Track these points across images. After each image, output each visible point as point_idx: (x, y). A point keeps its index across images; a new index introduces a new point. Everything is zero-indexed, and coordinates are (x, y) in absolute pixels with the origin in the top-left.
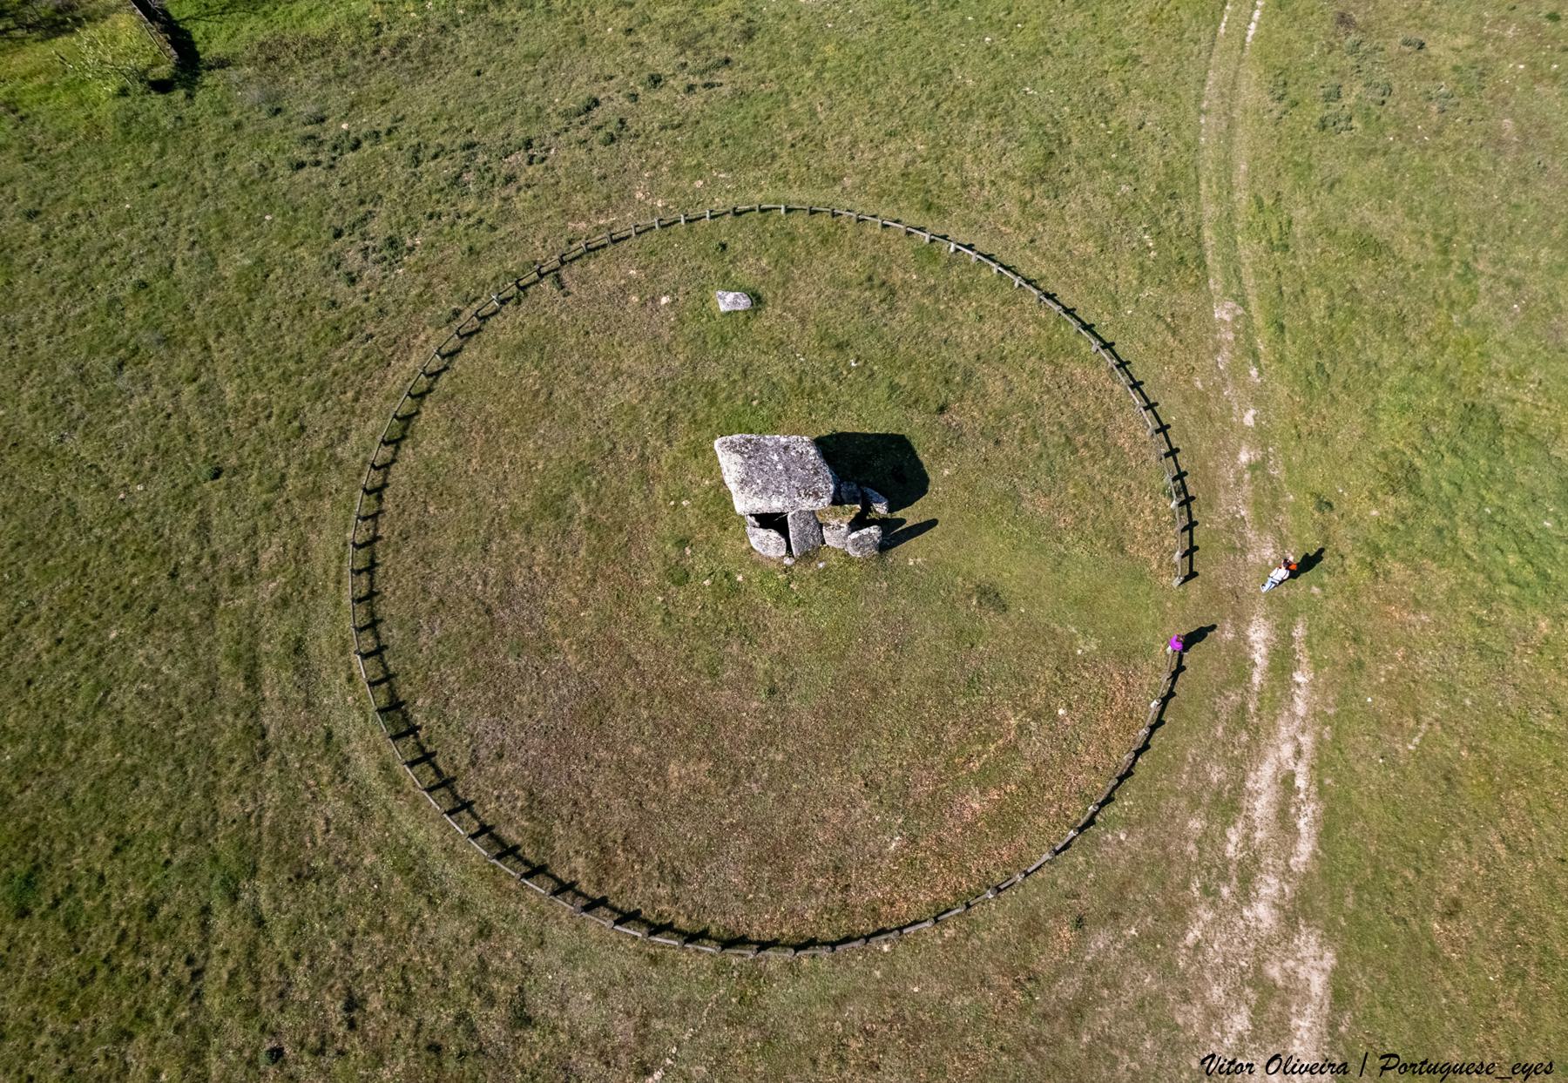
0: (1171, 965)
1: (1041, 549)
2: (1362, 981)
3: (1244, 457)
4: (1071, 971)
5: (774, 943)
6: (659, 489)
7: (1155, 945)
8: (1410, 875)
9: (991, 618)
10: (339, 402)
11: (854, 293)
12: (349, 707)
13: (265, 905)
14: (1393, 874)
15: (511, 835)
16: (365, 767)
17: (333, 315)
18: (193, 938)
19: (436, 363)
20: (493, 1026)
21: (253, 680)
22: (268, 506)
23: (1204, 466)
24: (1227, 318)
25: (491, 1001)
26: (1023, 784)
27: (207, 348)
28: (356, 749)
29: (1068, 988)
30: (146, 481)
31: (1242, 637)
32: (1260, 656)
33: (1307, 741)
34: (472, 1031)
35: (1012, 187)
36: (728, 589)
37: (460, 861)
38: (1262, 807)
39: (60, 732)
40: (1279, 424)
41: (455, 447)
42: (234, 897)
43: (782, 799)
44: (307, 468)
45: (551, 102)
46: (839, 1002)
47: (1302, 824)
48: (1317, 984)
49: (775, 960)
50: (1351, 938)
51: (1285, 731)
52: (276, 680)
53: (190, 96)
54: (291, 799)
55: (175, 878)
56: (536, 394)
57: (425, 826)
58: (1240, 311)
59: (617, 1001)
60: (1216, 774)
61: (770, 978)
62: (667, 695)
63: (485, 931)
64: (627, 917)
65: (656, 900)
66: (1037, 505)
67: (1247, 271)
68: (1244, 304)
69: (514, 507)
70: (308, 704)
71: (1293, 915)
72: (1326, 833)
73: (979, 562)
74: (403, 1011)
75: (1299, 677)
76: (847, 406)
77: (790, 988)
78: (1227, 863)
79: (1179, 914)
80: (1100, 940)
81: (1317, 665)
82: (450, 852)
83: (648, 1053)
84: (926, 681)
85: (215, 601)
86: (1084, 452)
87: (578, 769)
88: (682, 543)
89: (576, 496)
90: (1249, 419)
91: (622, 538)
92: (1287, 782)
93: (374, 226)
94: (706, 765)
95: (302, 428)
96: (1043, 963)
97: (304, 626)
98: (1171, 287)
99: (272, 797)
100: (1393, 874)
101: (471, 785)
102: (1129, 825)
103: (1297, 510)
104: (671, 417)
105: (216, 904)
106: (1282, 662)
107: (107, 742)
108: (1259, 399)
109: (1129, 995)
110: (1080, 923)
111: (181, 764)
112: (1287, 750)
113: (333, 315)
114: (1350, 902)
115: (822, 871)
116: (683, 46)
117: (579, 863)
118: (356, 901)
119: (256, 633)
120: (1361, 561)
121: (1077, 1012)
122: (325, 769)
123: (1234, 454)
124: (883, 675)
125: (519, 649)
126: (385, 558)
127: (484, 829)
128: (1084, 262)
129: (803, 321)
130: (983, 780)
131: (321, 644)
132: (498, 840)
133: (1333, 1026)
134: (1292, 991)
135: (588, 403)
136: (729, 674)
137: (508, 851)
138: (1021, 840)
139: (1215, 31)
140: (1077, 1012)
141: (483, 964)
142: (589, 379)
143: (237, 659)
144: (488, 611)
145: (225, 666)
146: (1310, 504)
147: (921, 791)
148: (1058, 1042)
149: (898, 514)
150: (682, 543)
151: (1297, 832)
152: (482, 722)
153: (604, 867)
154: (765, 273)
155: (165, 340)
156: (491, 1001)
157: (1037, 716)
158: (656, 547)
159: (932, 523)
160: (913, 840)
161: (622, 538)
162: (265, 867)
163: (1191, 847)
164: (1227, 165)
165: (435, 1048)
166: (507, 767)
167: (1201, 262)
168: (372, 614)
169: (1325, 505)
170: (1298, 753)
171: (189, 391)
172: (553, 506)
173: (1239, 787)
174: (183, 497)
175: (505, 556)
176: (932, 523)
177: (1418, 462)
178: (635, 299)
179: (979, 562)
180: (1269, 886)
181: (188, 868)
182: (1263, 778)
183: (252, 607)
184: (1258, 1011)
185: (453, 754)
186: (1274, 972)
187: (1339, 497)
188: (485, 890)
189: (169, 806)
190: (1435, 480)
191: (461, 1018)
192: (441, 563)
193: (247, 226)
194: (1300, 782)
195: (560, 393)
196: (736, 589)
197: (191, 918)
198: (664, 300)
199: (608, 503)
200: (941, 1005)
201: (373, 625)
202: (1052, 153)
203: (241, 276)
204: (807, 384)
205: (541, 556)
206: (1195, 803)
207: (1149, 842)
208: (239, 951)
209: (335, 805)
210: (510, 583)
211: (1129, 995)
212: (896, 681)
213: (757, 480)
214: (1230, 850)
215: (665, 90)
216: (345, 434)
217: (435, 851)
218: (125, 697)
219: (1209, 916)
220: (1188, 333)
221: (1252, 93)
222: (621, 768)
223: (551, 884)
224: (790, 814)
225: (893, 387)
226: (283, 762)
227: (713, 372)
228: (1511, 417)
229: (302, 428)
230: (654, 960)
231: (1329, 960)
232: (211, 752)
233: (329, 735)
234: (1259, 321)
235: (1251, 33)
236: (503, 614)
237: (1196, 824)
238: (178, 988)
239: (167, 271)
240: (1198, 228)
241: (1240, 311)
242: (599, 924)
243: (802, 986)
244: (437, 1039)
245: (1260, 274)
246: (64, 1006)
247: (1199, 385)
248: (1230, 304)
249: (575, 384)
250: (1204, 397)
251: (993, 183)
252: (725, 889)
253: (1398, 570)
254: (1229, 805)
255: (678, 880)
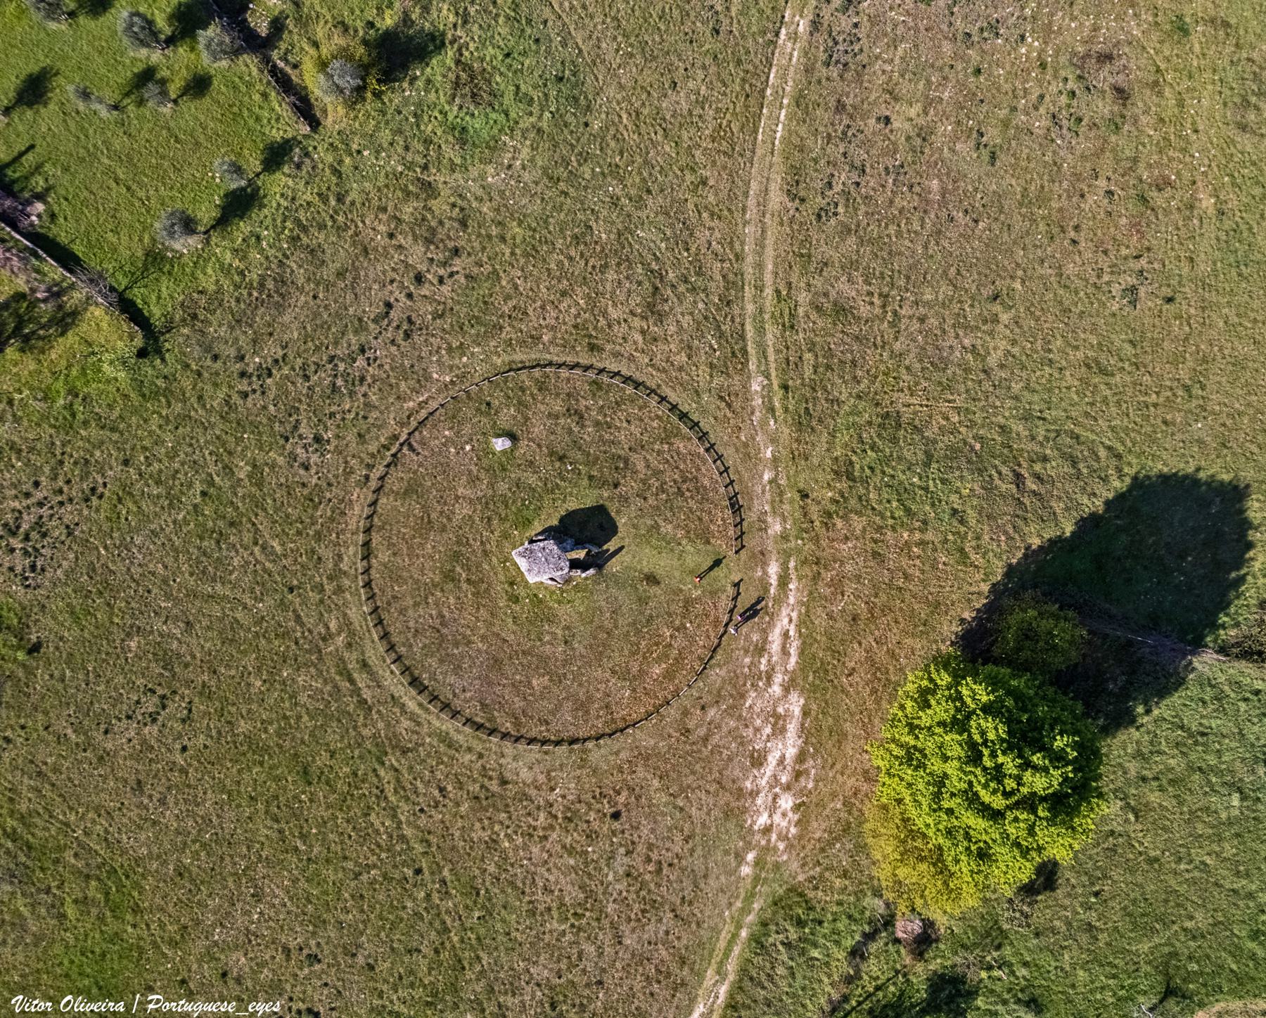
0: (740, 716)
1: (672, 550)
2: (814, 707)
3: (766, 477)
4: (702, 726)
5: (589, 738)
6: (494, 560)
7: (733, 710)
8: (835, 662)
9: (655, 590)
10: (330, 541)
11: (562, 421)
12: (394, 682)
13: (396, 764)
14: (829, 663)
15: (478, 719)
16: (412, 706)
17: (306, 492)
18: (375, 780)
19: (367, 511)
20: (494, 786)
21: (352, 681)
22: (322, 601)
23: (747, 487)
24: (759, 389)
25: (491, 778)
26: (676, 659)
27: (254, 524)
28: (405, 699)
29: (702, 732)
30: (262, 600)
31: (765, 573)
32: (774, 581)
33: (794, 615)
34: (487, 790)
35: (637, 322)
36: (537, 601)
37: (463, 735)
38: (775, 647)
39: (285, 717)
40: (784, 453)
41: (395, 554)
42: (383, 764)
43: (580, 685)
44: (330, 578)
45: (364, 311)
46: (617, 754)
47: (792, 651)
48: (797, 711)
49: (590, 745)
50: (811, 692)
51: (784, 612)
52: (361, 679)
53: (163, 360)
54: (388, 725)
55: (358, 762)
56: (422, 518)
57: (445, 724)
58: (766, 382)
59: (536, 769)
60: (755, 637)
61: (590, 751)
62: (524, 653)
63: (481, 756)
64: (531, 741)
65: (541, 732)
66: (667, 529)
67: (770, 351)
68: (768, 377)
69: (432, 580)
70: (379, 686)
71: (786, 690)
72: (802, 653)
73: (645, 563)
74: (461, 789)
75: (791, 586)
76: (571, 494)
77: (598, 754)
78: (761, 673)
79: (743, 696)
80: (712, 712)
81: (800, 579)
82: (458, 731)
83: (553, 783)
84: (629, 625)
85: (320, 651)
86: (688, 494)
87: (498, 689)
88: (512, 584)
89: (458, 569)
90: (769, 454)
91: (484, 586)
92: (786, 635)
93: (303, 430)
94: (547, 678)
95: (319, 559)
96: (691, 725)
97: (363, 653)
98: (728, 374)
99: (381, 725)
100: (829, 663)
101: (457, 704)
102: (719, 666)
103: (792, 501)
104: (489, 519)
105: (377, 767)
106: (784, 581)
107: (305, 718)
108: (774, 441)
109: (725, 729)
110: (703, 708)
111: (339, 721)
112: (786, 621)
113: (306, 492)
114: (811, 678)
115: (601, 708)
116: (429, 241)
117: (508, 725)
118: (429, 755)
119: (344, 662)
120: (822, 522)
121: (705, 740)
122: (396, 710)
123: (761, 477)
124: (610, 626)
125: (457, 645)
126: (385, 615)
127: (468, 720)
128: (681, 369)
129: (539, 446)
130: (658, 660)
131: (373, 660)
132: (475, 723)
133: (802, 725)
134: (788, 715)
135: (449, 519)
136: (547, 638)
137: (479, 727)
138: (677, 681)
139: (756, 139)
140: (705, 740)
141: (484, 767)
142: (445, 503)
143: (341, 674)
144: (438, 631)
145: (338, 678)
146: (797, 497)
147: (635, 670)
148: (700, 751)
149: (605, 547)
150: (512, 584)
151: (790, 654)
152: (451, 679)
153: (517, 724)
154: (515, 418)
155: (232, 524)
156: (491, 778)
157: (678, 630)
158: (499, 588)
159: (622, 548)
160: (634, 690)
161: (484, 586)
162: (389, 751)
163: (746, 669)
164: (760, 266)
165: (476, 798)
166: (468, 695)
167: (744, 351)
168: (389, 643)
169: (804, 496)
170: (791, 621)
171: (257, 550)
172: (449, 576)
173: (765, 641)
174: (282, 605)
175: (437, 604)
176: (622, 548)
177: (854, 458)
178: (453, 450)
179: (645, 563)
180: (778, 678)
181: (361, 757)
182: (775, 637)
183: (337, 650)
184: (774, 726)
185: (446, 694)
186: (780, 710)
187: (812, 490)
188: (476, 742)
189: (342, 737)
190: (862, 468)
191: (482, 787)
192: (410, 612)
193: (237, 444)
194: (791, 633)
195: (434, 516)
196: (540, 601)
197: (371, 774)
198: (468, 448)
199: (474, 570)
200: (655, 746)
201: (391, 647)
202: (657, 288)
203: (250, 476)
204: (549, 485)
205: (452, 601)
206: (746, 651)
207: (729, 672)
208: (393, 781)
209: (406, 723)
210: (443, 617)
211: (725, 729)
212: (616, 627)
213: (540, 568)
214: (762, 667)
215: (427, 285)
216: (340, 556)
217: (452, 732)
218: (303, 698)
219: (754, 695)
220: (737, 405)
221: (777, 198)
222: (513, 685)
223: (499, 735)
224: (584, 690)
225: (591, 478)
226: (379, 712)
227: (502, 487)
228: (906, 415)
229: (319, 559)
230: (546, 753)
231: (802, 701)
232: (349, 713)
233: (393, 697)
234: (776, 387)
235: (778, 135)
236: (445, 631)
237: (747, 660)
238: (377, 797)
239: (211, 483)
240: (743, 325)
241: (766, 382)
242: (521, 746)
243: (603, 751)
244: (392, 300)
245: (778, 352)
246: (341, 810)
247: (743, 438)
248: (760, 379)
249: (439, 508)
250: (746, 445)
251: (625, 321)
252: (566, 721)
253: (839, 523)
254: (761, 650)
255: (547, 723)
